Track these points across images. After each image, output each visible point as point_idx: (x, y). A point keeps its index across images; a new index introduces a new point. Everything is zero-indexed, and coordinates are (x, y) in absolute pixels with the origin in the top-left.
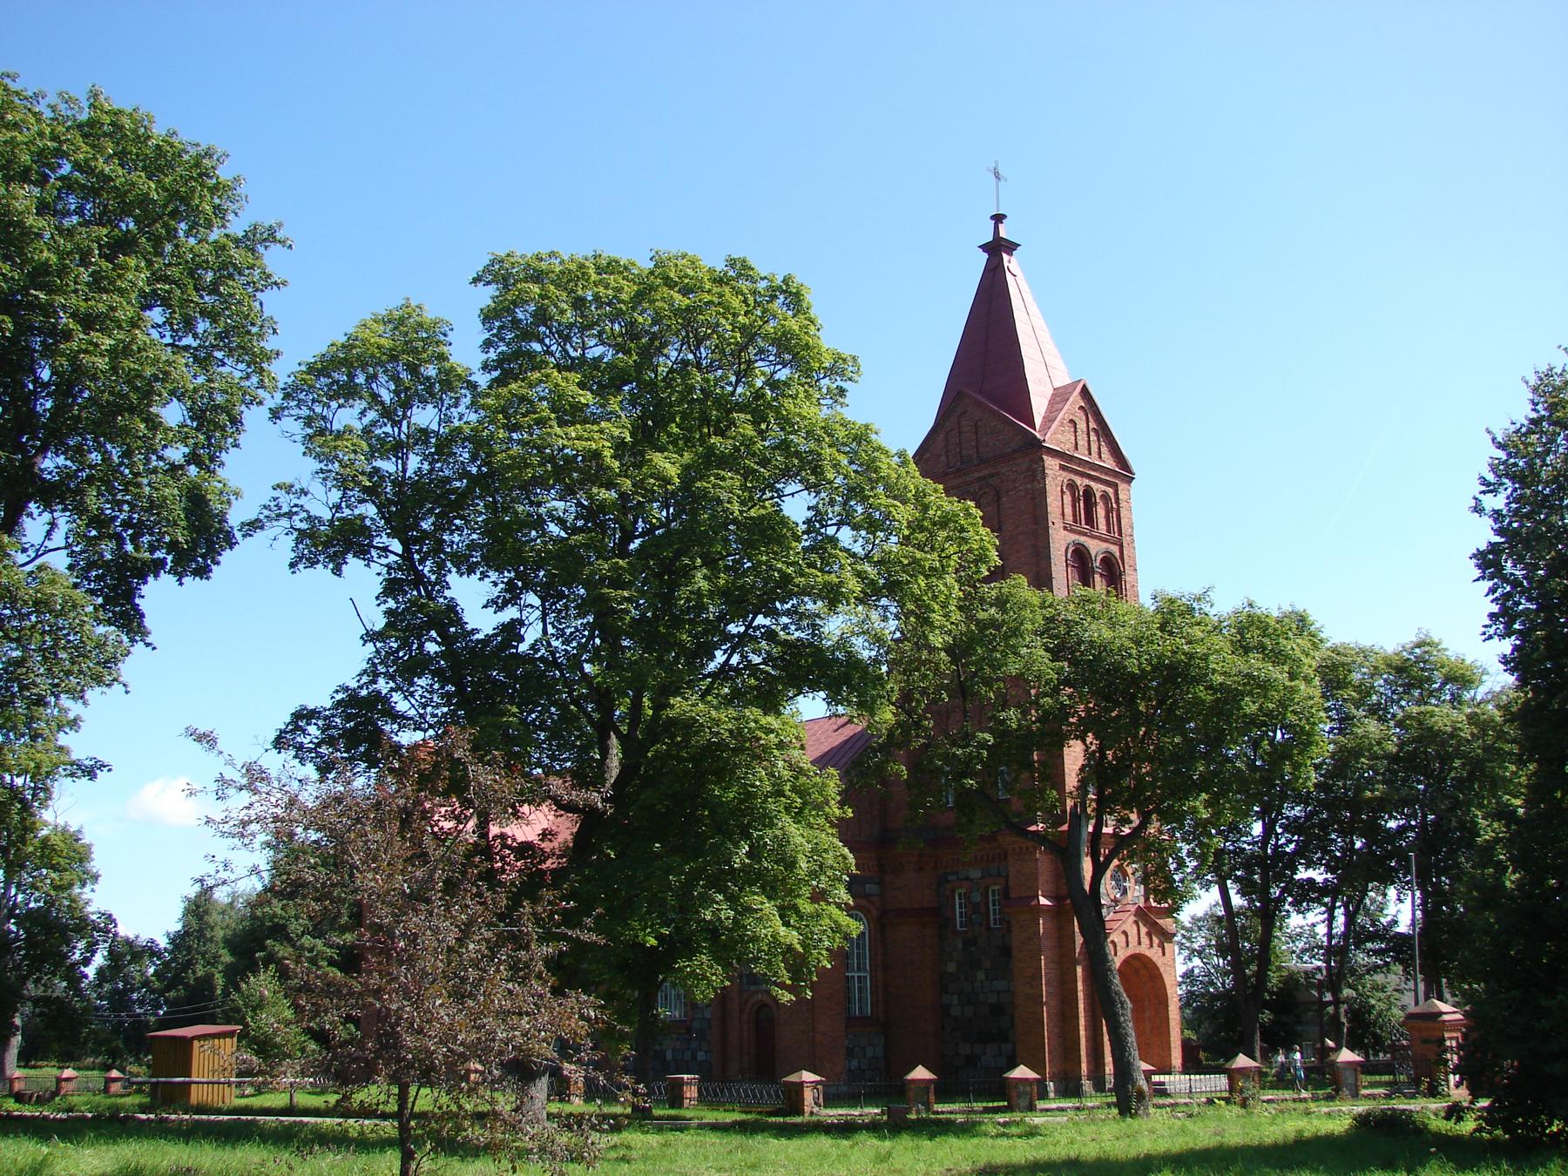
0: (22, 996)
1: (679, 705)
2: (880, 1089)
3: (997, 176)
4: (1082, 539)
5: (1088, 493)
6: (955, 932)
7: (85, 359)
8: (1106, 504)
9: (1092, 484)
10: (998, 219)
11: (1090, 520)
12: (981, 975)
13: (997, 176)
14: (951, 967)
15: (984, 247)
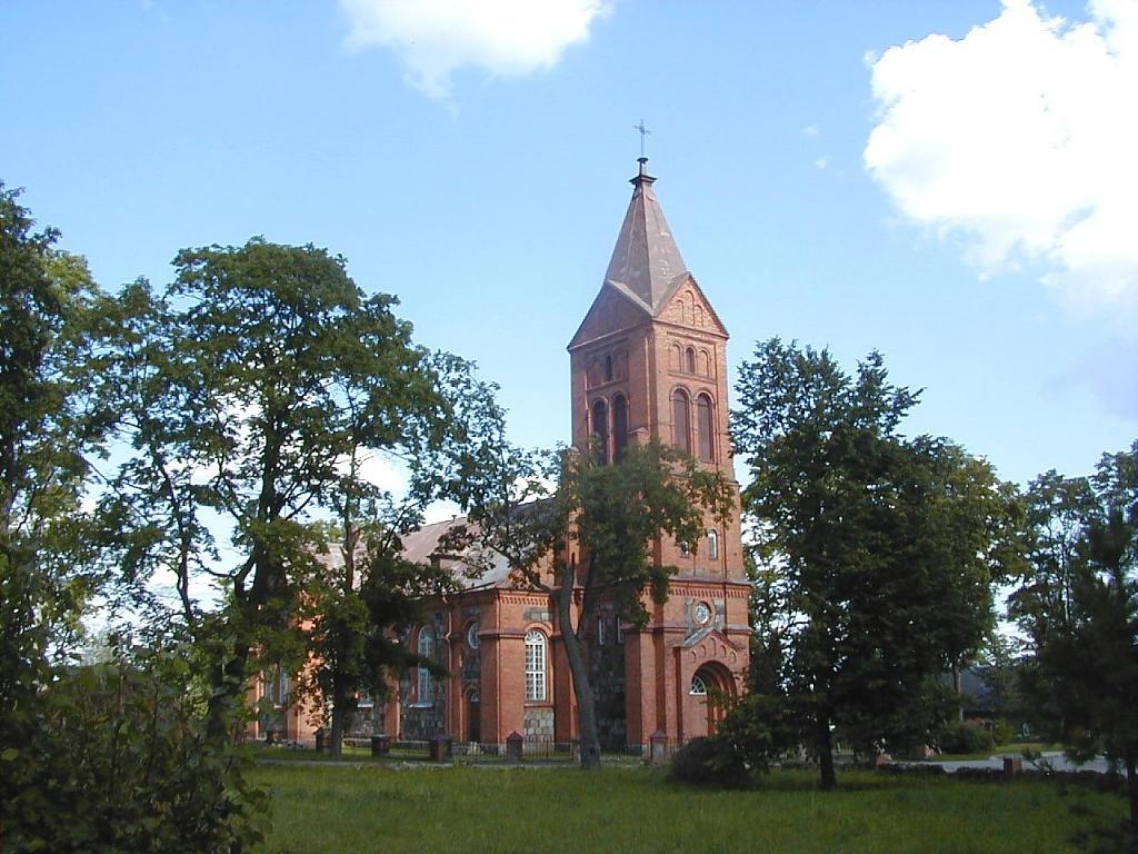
0: (994, 615)
1: (72, 381)
2: (339, 851)
3: (642, 131)
4: (685, 382)
5: (690, 351)
6: (598, 645)
7: (244, 480)
8: (719, 672)
9: (695, 343)
10: (643, 161)
11: (692, 368)
12: (611, 674)
13: (642, 131)
14: (596, 668)
15: (633, 181)
